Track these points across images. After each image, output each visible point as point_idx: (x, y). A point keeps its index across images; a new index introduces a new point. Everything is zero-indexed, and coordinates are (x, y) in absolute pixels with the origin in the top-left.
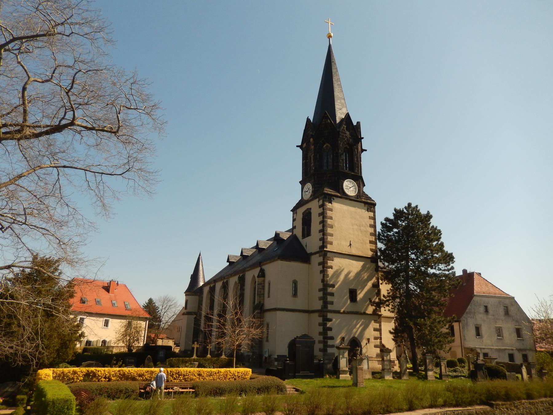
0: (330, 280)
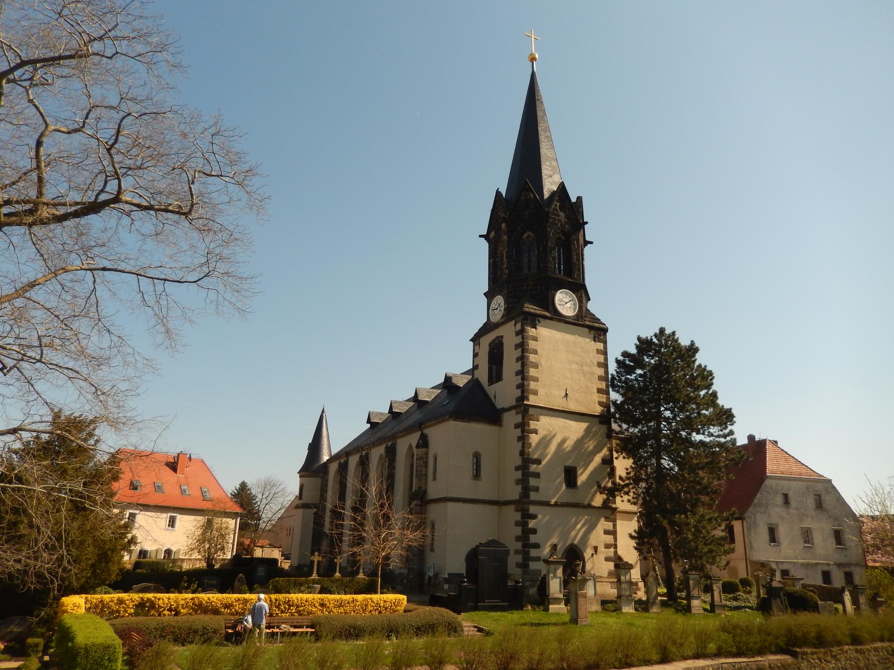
0: (534, 452)
